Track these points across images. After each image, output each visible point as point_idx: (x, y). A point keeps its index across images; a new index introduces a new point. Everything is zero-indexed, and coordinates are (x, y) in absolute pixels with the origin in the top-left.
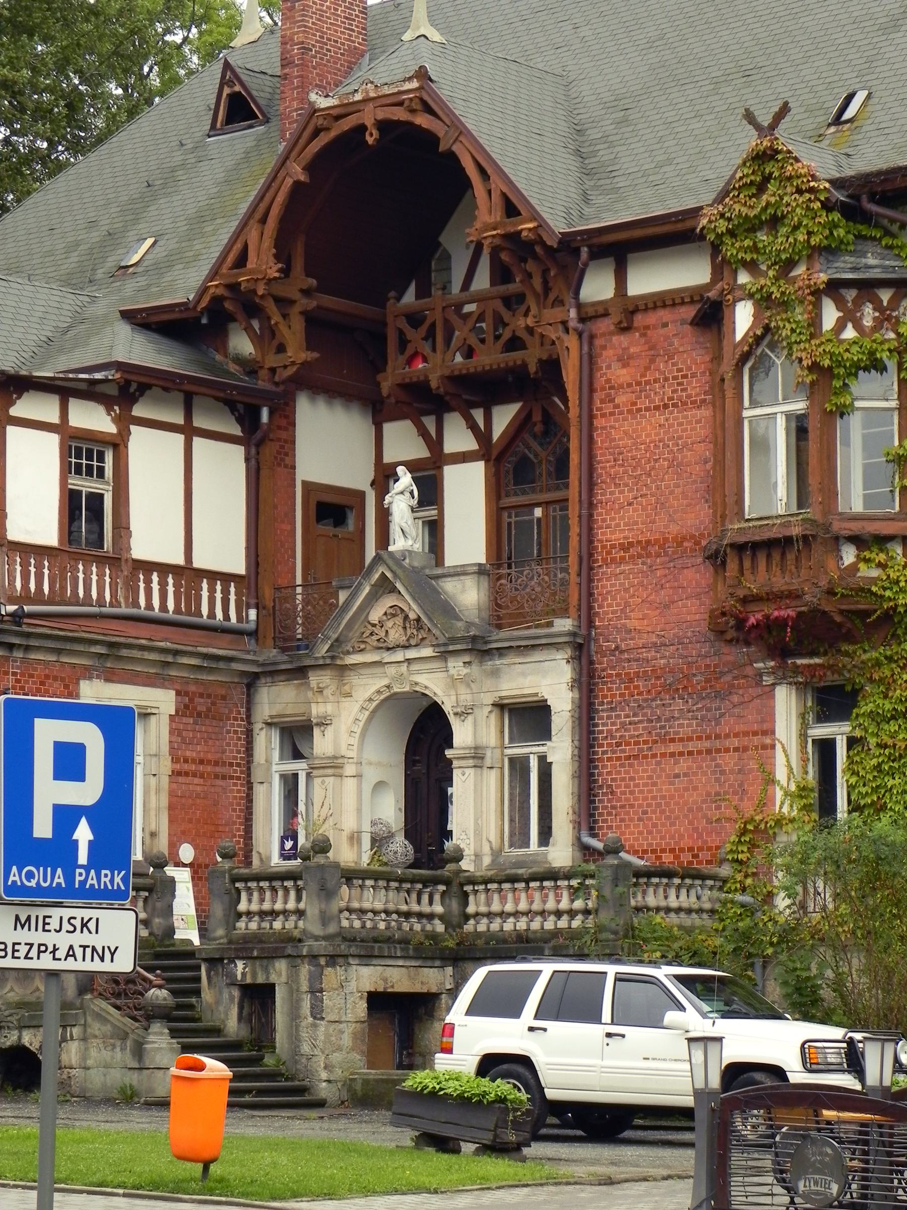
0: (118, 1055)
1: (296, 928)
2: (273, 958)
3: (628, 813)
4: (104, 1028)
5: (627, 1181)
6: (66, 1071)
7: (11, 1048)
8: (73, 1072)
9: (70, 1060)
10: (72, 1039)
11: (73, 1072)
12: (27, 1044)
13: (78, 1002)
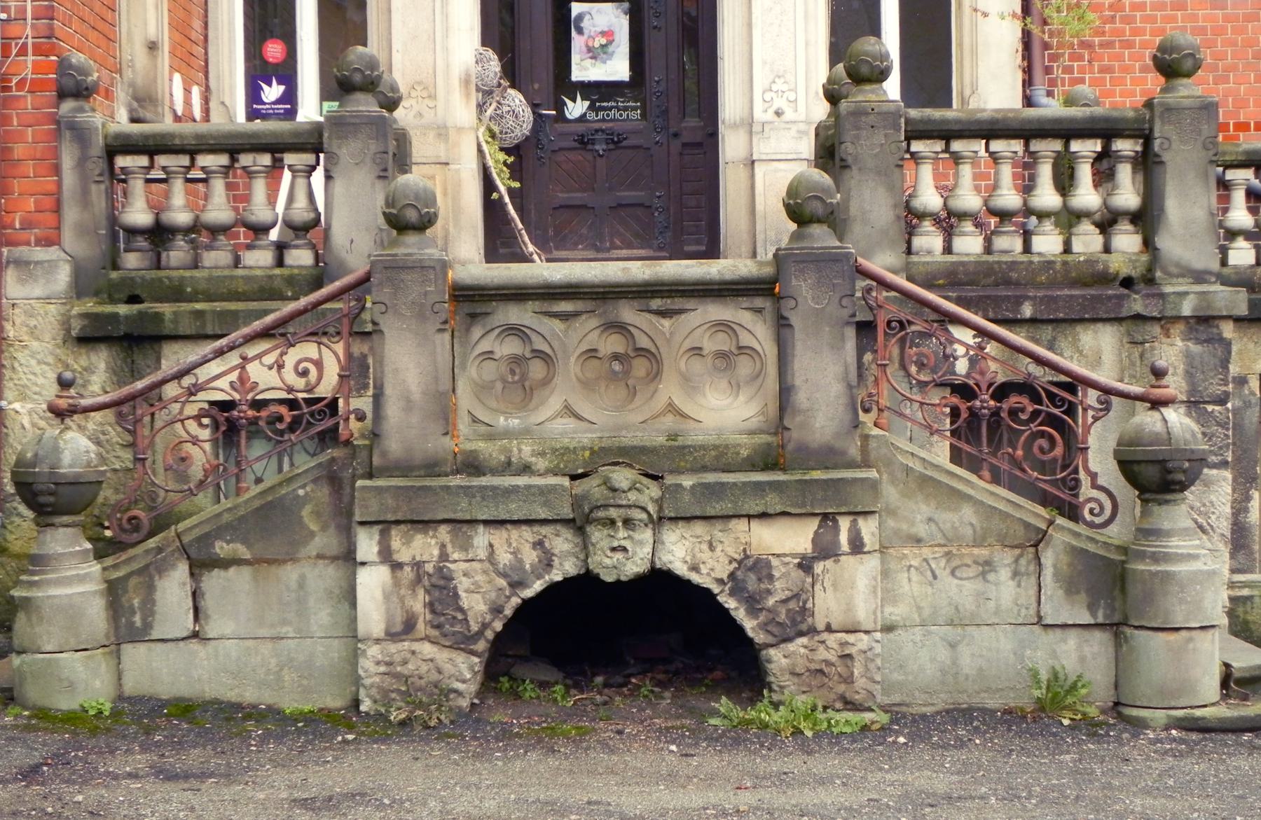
0: (1006, 590)
1: (1107, 249)
2: (1082, 321)
3: (1119, 58)
4: (948, 518)
5: (177, 640)
6: (832, 640)
7: (639, 580)
8: (861, 642)
9: (850, 608)
10: (857, 546)
11: (861, 642)
12: (681, 569)
13: (854, 451)
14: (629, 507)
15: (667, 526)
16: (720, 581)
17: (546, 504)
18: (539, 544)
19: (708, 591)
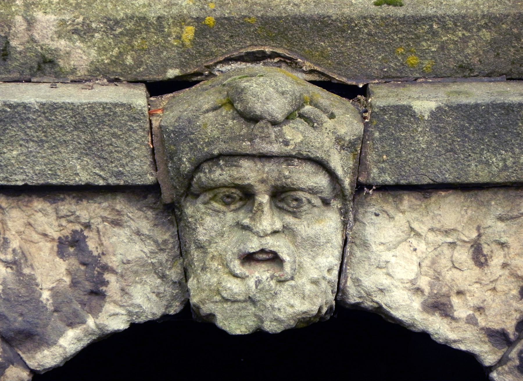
7: (307, 332)
12: (406, 307)
14: (288, 158)
15: (376, 203)
16: (498, 337)
17: (91, 149)
18: (71, 244)
19: (470, 359)
